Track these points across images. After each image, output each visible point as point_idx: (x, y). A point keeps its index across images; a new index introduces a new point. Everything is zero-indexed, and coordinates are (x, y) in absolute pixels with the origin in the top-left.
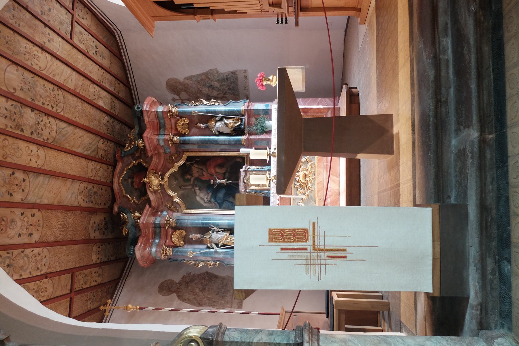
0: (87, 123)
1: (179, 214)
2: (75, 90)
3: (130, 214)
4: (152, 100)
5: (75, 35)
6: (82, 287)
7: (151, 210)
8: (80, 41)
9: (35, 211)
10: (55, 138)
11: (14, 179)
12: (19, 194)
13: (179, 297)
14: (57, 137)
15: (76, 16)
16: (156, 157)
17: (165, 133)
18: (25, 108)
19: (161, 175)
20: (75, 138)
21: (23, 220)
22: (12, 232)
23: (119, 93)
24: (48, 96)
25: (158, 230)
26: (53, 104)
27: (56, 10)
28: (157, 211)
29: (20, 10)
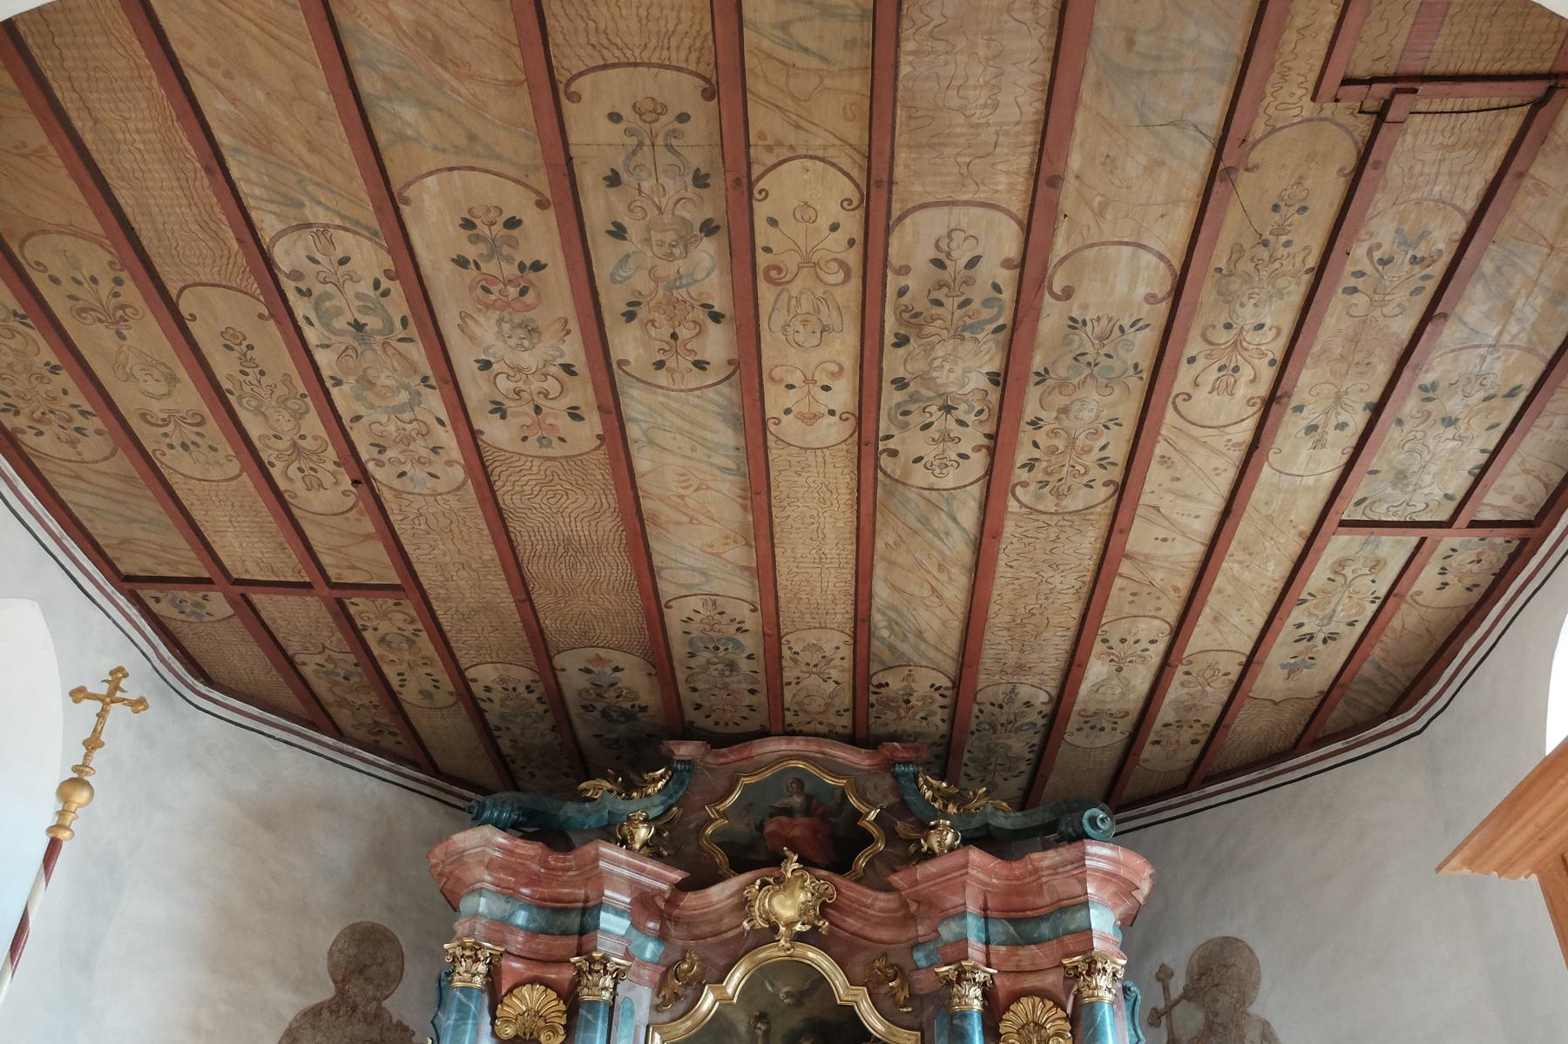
0: (998, 617)
1: (643, 1012)
2: (1127, 556)
3: (662, 803)
4: (1138, 884)
5: (1363, 538)
6: (365, 629)
7: (661, 892)
8: (1341, 564)
9: (593, 425)
10: (904, 484)
11: (695, 322)
12: (642, 351)
13: (313, 1014)
14: (912, 494)
15: (1449, 540)
16: (893, 905)
17: (993, 947)
18: (997, 343)
19: (815, 928)
20: (929, 572)
21: (545, 375)
22: (487, 328)
23: (1158, 742)
24: (1072, 442)
25: (574, 921)
26: (1044, 464)
27: (1453, 450)
28: (663, 917)
29: (1417, 291)
